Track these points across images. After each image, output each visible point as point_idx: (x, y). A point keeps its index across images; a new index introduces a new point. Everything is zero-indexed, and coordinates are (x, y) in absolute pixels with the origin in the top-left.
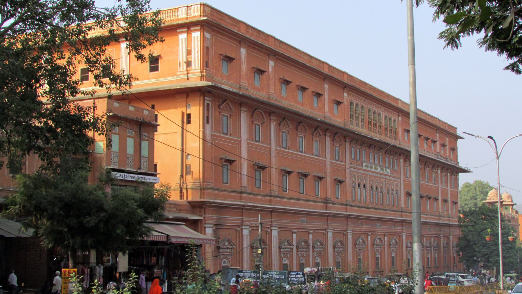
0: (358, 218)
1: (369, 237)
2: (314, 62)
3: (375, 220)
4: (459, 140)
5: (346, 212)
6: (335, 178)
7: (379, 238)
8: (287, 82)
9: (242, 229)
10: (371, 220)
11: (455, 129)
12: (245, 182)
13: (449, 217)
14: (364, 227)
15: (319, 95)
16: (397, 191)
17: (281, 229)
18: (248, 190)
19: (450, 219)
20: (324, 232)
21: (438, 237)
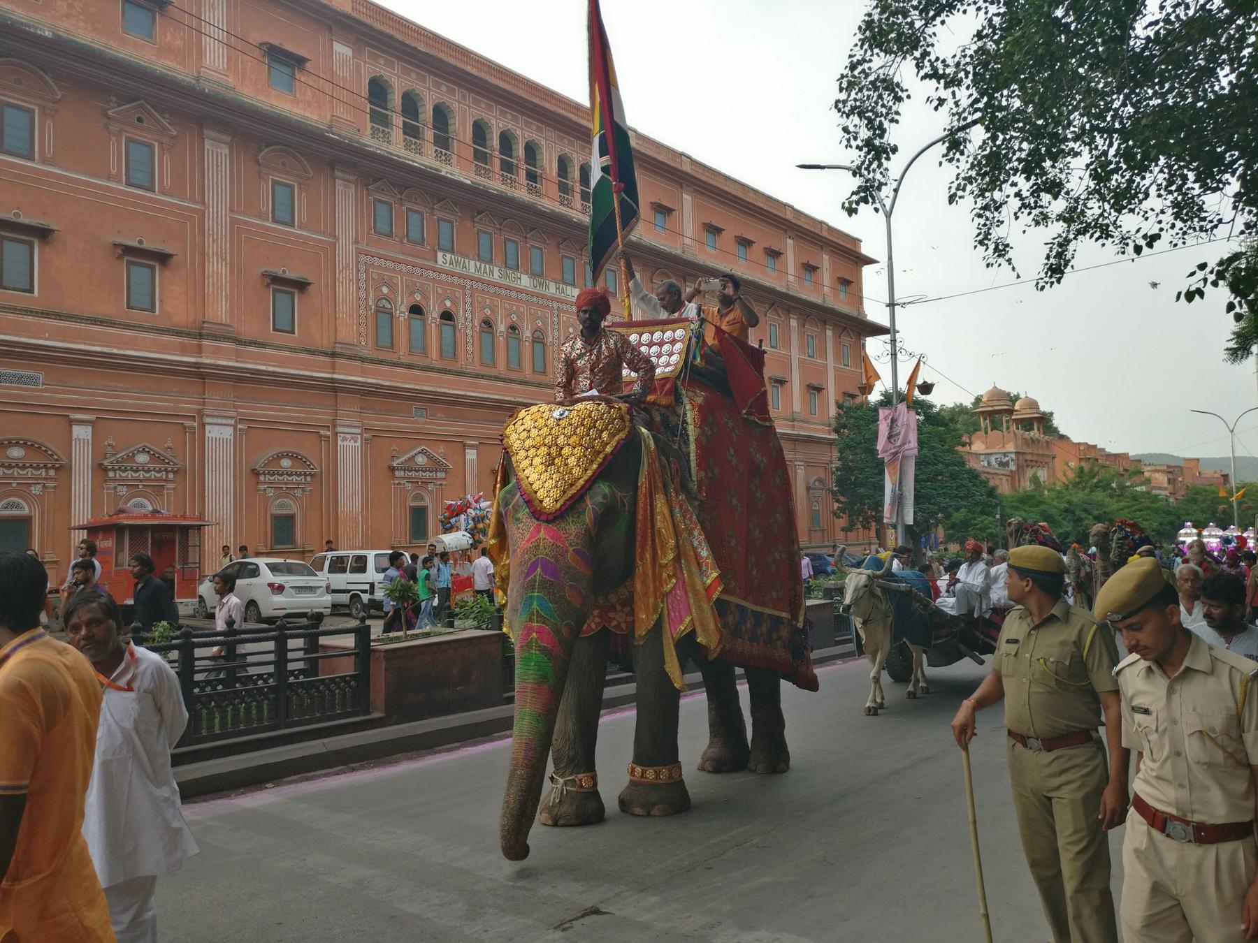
9: (203, 425)
20: (187, 423)
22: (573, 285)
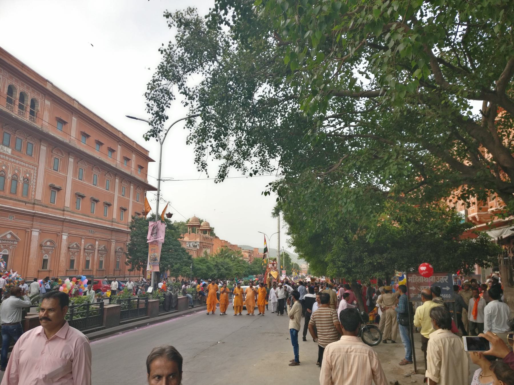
0: (70, 222)
1: (83, 240)
2: (105, 124)
3: (9, 212)
4: (150, 163)
5: (34, 210)
6: (50, 184)
7: (10, 233)
8: (87, 136)
9: (32, 231)
10: (78, 224)
11: (147, 152)
12: (115, 216)
13: (64, 211)
14: (81, 232)
15: (112, 151)
16: (27, 181)
17: (70, 235)
18: (117, 221)
19: (65, 212)
21: (109, 242)
22: (8, 146)
